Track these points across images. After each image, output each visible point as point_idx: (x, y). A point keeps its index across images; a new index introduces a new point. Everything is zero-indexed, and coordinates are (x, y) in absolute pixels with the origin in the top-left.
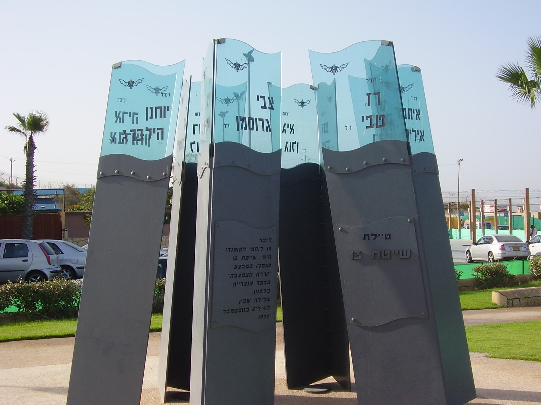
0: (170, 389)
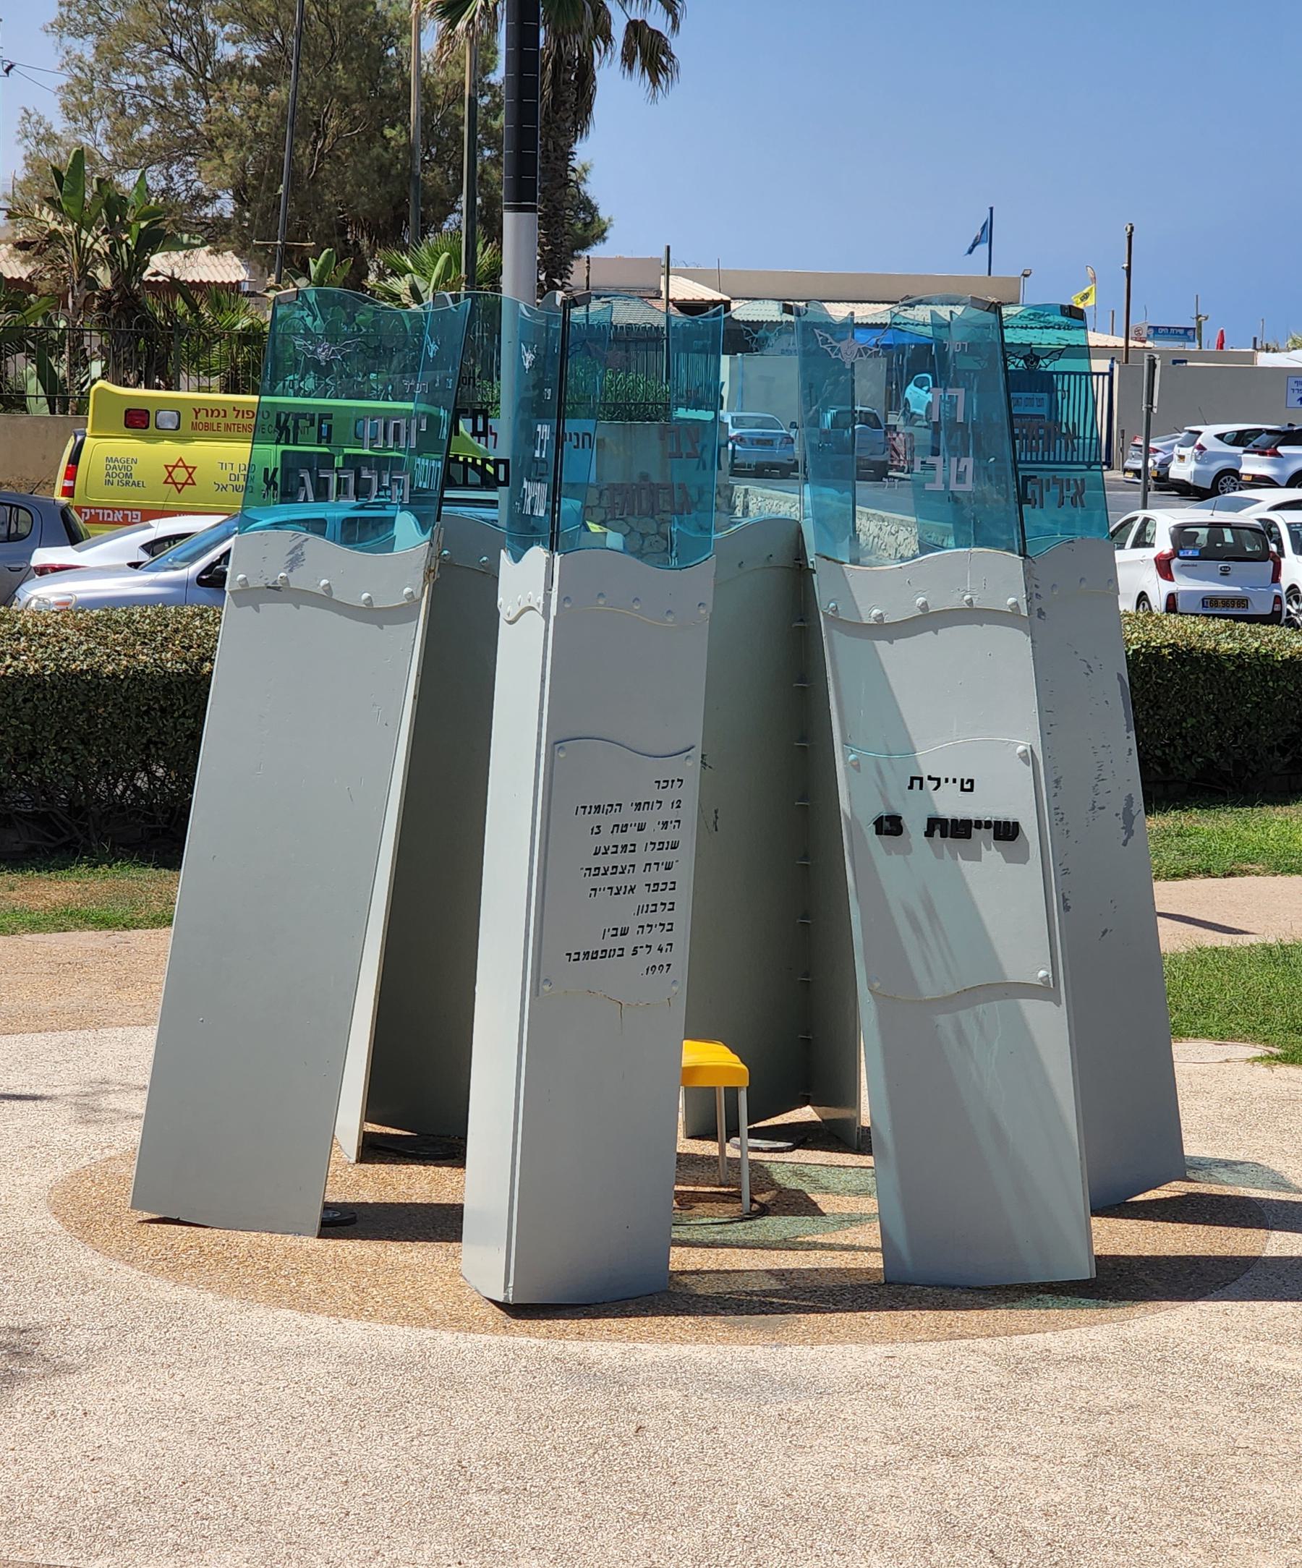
0: (371, 1128)
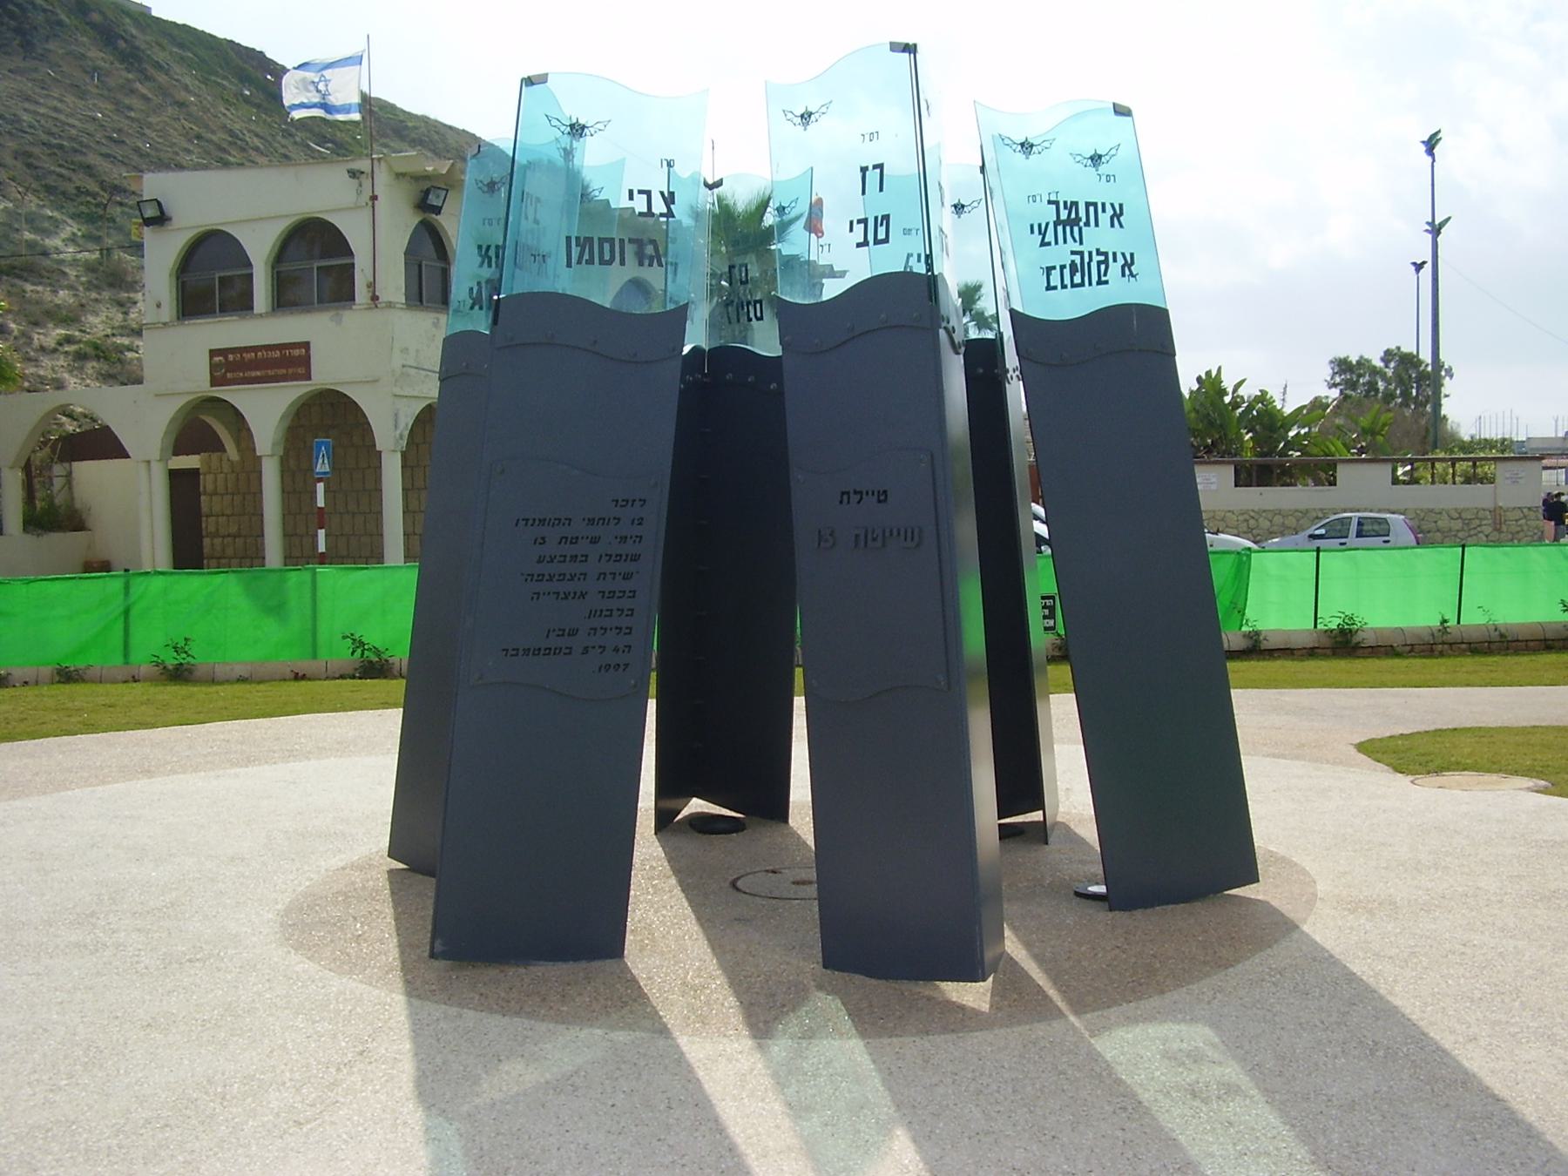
0: (1036, 816)
